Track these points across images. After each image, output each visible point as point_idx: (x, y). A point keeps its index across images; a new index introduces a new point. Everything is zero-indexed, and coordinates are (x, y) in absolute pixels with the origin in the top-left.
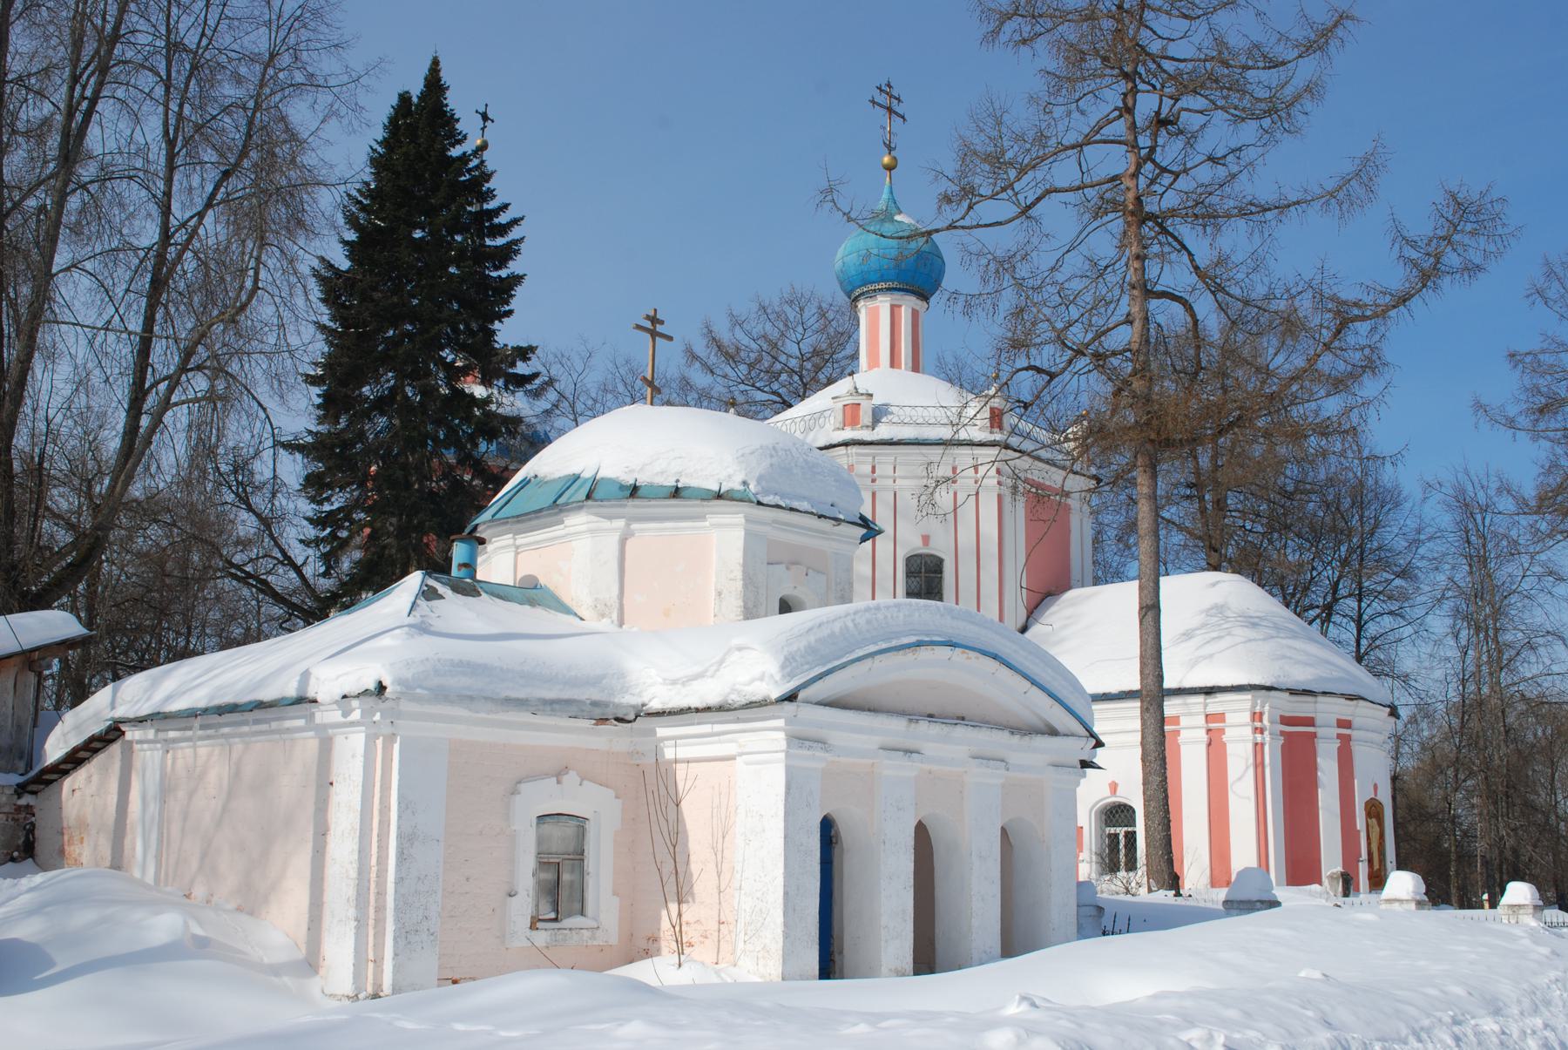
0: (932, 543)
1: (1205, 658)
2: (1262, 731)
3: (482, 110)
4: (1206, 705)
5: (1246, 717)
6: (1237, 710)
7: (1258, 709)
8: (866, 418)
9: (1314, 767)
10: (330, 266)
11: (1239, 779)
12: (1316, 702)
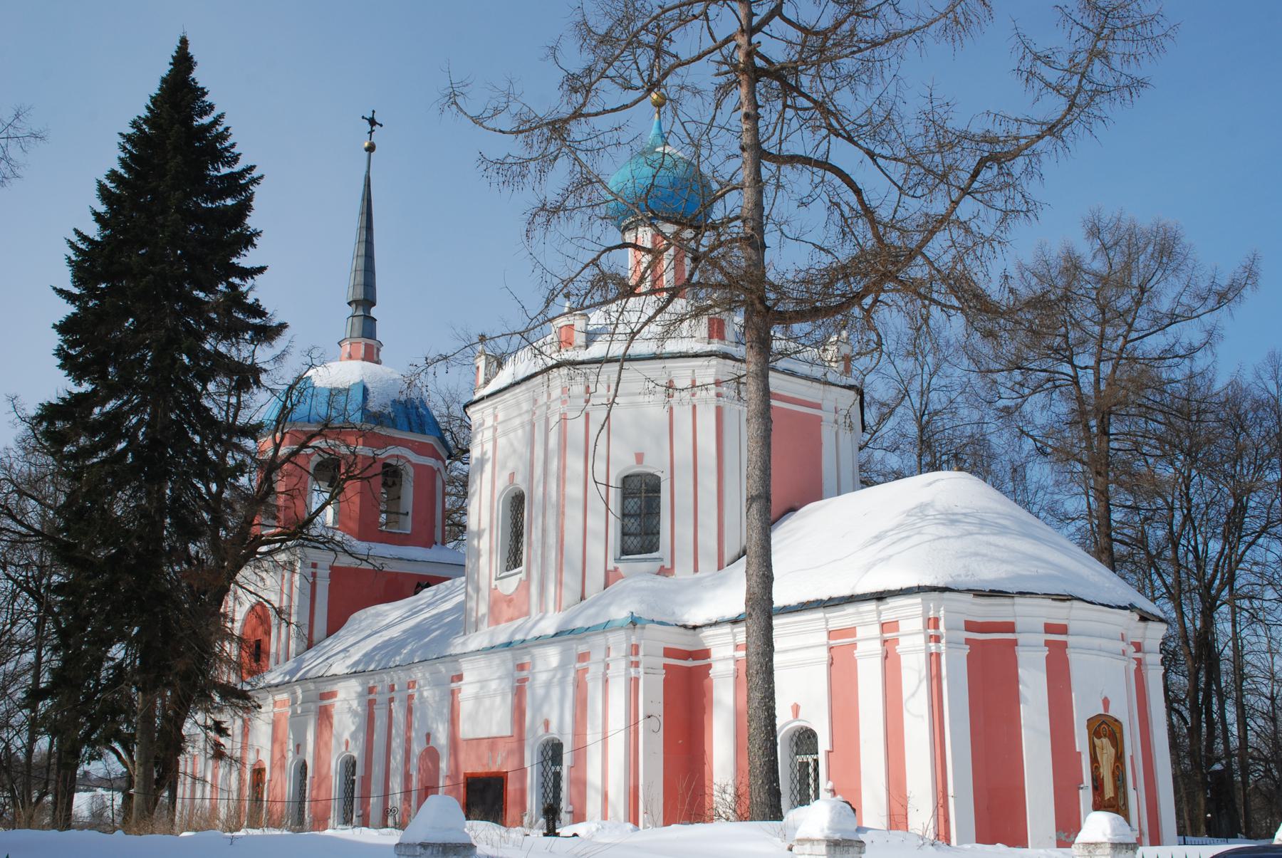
0: (647, 460)
1: (882, 560)
2: (937, 639)
3: (369, 115)
4: (879, 614)
5: (918, 624)
6: (909, 614)
7: (931, 615)
8: (580, 339)
9: (1014, 680)
10: (84, 238)
11: (913, 695)
12: (1013, 605)
